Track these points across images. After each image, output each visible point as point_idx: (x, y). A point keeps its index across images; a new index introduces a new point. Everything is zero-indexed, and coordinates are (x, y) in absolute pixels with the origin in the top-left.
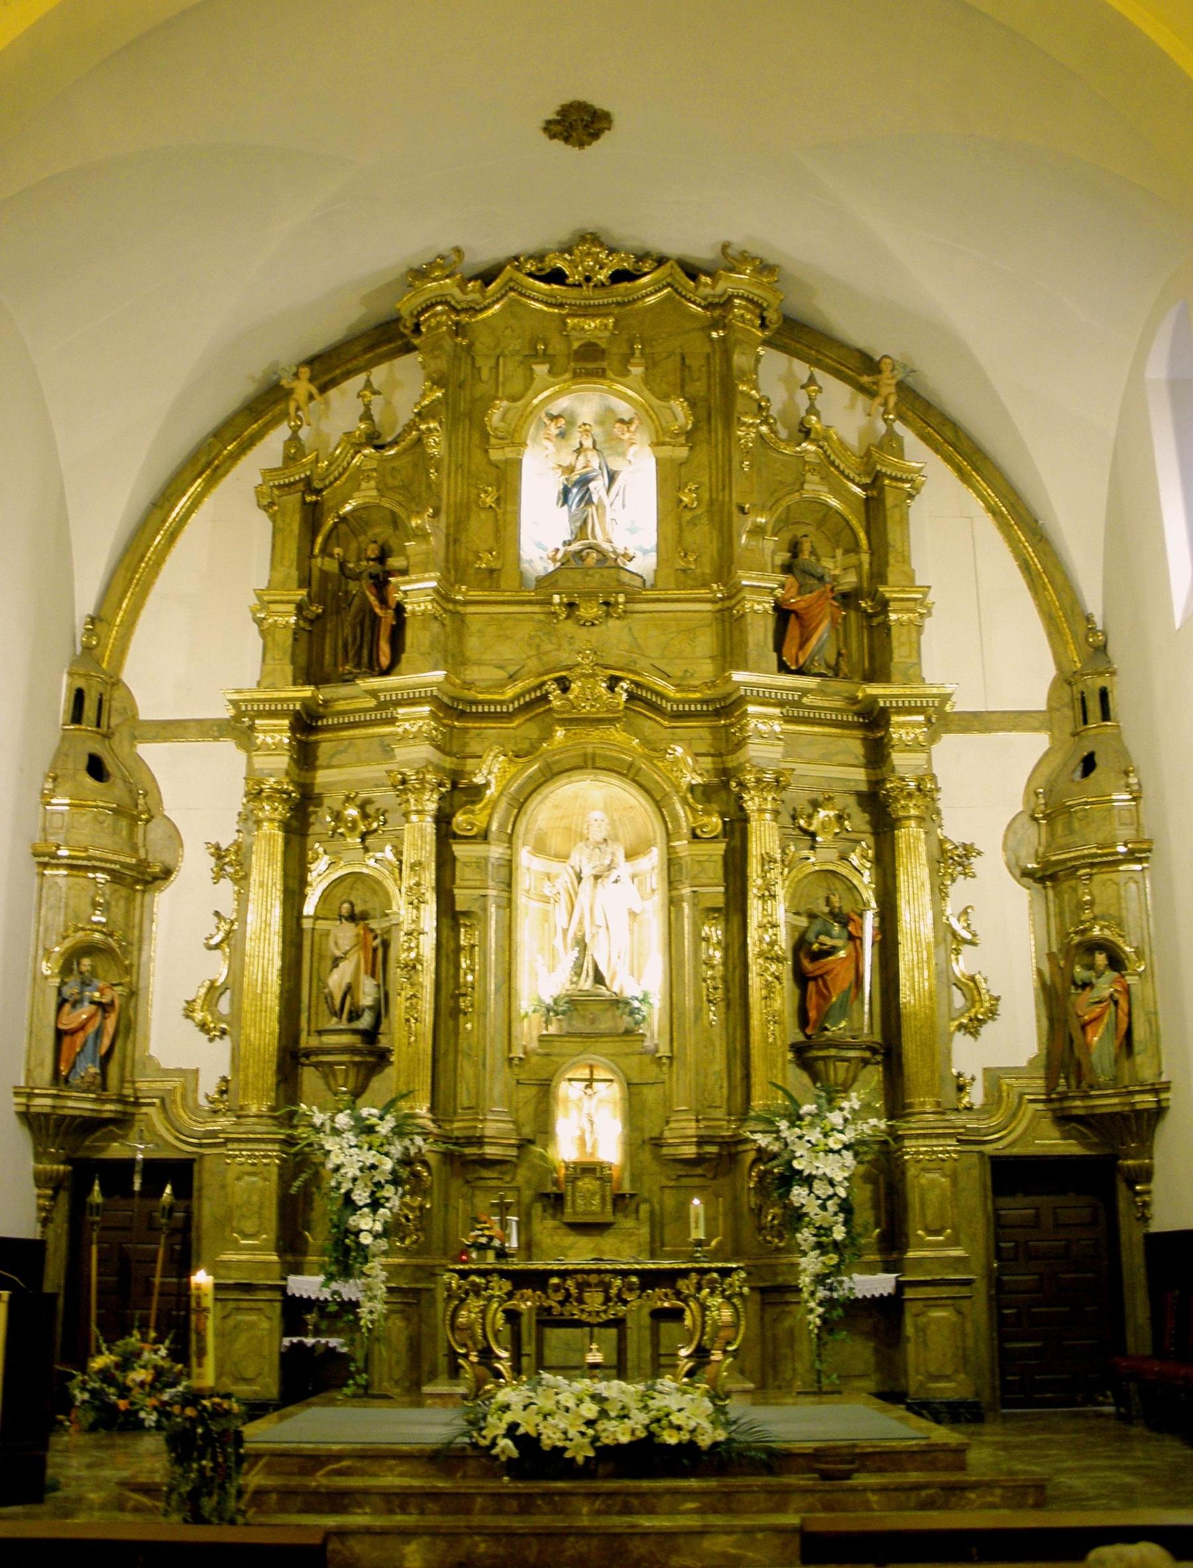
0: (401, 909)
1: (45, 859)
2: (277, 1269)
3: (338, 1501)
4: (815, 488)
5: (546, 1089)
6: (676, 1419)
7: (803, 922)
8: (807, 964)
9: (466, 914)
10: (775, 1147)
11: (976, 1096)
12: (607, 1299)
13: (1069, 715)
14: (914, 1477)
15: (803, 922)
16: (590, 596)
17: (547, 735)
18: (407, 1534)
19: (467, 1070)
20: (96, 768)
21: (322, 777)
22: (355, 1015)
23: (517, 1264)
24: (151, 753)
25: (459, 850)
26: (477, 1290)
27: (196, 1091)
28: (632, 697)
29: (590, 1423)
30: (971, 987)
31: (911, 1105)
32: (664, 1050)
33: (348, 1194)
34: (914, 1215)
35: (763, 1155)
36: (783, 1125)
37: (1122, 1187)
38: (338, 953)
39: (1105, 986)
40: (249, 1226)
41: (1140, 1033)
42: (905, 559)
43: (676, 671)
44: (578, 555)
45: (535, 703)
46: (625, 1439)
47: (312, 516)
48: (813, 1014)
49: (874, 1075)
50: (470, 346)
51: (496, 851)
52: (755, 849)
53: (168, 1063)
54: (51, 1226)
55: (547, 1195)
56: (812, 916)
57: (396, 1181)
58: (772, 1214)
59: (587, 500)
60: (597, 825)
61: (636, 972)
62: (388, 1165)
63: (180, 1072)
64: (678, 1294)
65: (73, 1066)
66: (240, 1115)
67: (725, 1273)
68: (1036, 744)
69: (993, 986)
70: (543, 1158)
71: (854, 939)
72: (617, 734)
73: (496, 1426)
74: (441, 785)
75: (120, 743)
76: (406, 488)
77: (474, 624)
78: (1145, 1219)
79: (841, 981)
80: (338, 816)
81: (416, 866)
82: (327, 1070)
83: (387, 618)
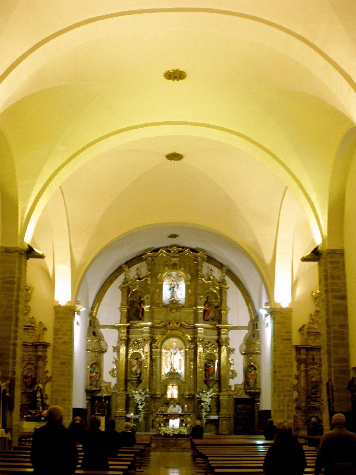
1: (87, 350)
6: (183, 431)
7: (206, 361)
9: (154, 360)
10: (200, 397)
11: (233, 389)
13: (251, 328)
16: (174, 309)
19: (154, 384)
20: (94, 334)
21: (131, 336)
22: (137, 374)
23: (164, 414)
24: (102, 330)
25: (153, 350)
26: (159, 416)
28: (180, 326)
29: (173, 432)
30: (233, 371)
31: (222, 390)
32: (184, 381)
35: (198, 398)
38: (134, 365)
39: (253, 373)
40: (121, 407)
41: (258, 380)
42: (226, 302)
43: (187, 321)
44: (172, 301)
46: (176, 434)
47: (129, 291)
48: (207, 376)
49: (217, 385)
51: (159, 350)
52: (199, 351)
54: (88, 407)
55: (166, 403)
56: (208, 360)
57: (144, 401)
58: (199, 406)
59: (173, 291)
61: (180, 369)
62: (144, 399)
63: (108, 383)
64: (183, 417)
67: (189, 415)
68: (246, 331)
69: (237, 371)
70: (165, 397)
71: (214, 364)
73: (162, 432)
74: (150, 340)
75: (97, 328)
78: (258, 408)
79: (211, 371)
81: (147, 353)
82: (132, 383)
83: (141, 310)
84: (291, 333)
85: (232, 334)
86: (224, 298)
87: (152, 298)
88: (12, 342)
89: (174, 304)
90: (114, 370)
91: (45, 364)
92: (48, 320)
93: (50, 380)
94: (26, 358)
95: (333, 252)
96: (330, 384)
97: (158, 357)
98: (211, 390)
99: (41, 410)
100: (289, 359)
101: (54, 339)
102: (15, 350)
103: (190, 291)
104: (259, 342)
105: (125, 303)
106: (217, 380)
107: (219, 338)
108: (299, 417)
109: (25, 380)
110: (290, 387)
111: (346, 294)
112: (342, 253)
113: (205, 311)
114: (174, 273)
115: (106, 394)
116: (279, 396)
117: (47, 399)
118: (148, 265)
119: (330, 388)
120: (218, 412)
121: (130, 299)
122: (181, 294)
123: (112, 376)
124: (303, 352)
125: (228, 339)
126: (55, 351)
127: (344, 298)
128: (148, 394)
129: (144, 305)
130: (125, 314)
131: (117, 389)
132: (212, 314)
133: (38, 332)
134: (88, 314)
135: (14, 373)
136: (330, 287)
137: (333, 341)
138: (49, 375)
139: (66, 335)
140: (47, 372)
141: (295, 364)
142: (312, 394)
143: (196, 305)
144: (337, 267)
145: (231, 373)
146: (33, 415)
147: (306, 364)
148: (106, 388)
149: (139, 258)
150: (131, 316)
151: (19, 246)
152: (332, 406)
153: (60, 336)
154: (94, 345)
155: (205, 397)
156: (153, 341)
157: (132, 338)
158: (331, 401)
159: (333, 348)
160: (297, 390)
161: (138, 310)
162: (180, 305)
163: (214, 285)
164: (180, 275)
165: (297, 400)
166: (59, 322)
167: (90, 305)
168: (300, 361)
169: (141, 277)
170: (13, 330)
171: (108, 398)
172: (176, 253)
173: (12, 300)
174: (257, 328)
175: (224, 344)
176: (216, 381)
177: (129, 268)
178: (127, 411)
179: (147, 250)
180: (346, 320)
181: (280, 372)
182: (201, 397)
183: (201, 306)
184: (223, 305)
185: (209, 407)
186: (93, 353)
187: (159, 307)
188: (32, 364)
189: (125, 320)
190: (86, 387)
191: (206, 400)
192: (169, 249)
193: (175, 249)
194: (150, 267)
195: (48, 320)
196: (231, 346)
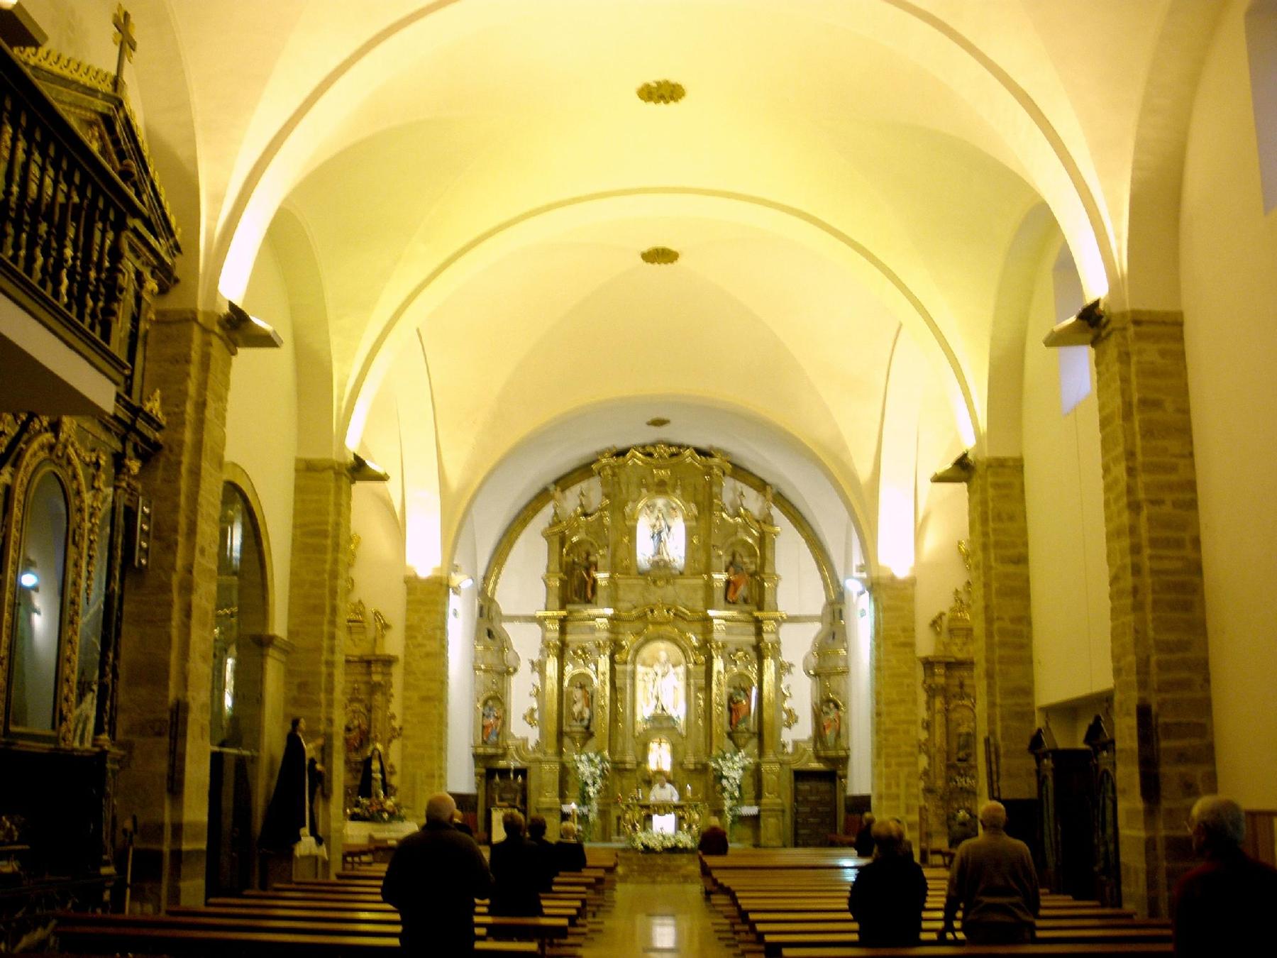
0: (596, 682)
1: (476, 668)
5: (645, 747)
7: (732, 690)
8: (732, 705)
9: (621, 688)
10: (717, 767)
13: (829, 619)
15: (732, 690)
16: (661, 578)
17: (646, 627)
24: (507, 627)
30: (790, 713)
32: (684, 733)
35: (715, 770)
36: (720, 760)
39: (832, 715)
41: (843, 730)
42: (773, 564)
43: (690, 604)
44: (657, 562)
45: (642, 617)
49: (755, 741)
51: (629, 667)
53: (518, 735)
56: (735, 688)
57: (600, 776)
59: (660, 540)
60: (663, 656)
66: (545, 753)
68: (817, 626)
71: (748, 697)
72: (668, 628)
75: (496, 623)
78: (844, 790)
80: (575, 653)
81: (604, 674)
82: (573, 740)
83: (590, 582)
85: (787, 632)
86: (768, 554)
88: (323, 658)
89: (661, 570)
91: (389, 701)
92: (393, 608)
96: (992, 741)
97: (628, 681)
100: (908, 686)
101: (407, 646)
102: (330, 675)
110: (913, 746)
111: (1027, 552)
113: (728, 582)
114: (660, 502)
116: (888, 765)
117: (392, 773)
119: (992, 749)
120: (758, 797)
121: (565, 559)
122: (676, 550)
126: (408, 671)
127: (1022, 560)
129: (596, 570)
132: (743, 590)
135: (330, 721)
136: (992, 538)
139: (432, 638)
140: (393, 717)
141: (922, 697)
142: (959, 760)
145: (785, 716)
147: (945, 697)
149: (584, 470)
151: (334, 457)
152: (995, 787)
153: (420, 639)
154: (491, 659)
156: (616, 647)
159: (997, 667)
160: (927, 753)
163: (746, 527)
165: (926, 773)
167: (481, 572)
168: (932, 692)
169: (589, 511)
171: (522, 772)
177: (563, 491)
178: (563, 797)
179: (602, 453)
180: (1027, 606)
183: (720, 572)
184: (767, 570)
188: (360, 701)
190: (475, 747)
195: (393, 608)
196: (786, 657)
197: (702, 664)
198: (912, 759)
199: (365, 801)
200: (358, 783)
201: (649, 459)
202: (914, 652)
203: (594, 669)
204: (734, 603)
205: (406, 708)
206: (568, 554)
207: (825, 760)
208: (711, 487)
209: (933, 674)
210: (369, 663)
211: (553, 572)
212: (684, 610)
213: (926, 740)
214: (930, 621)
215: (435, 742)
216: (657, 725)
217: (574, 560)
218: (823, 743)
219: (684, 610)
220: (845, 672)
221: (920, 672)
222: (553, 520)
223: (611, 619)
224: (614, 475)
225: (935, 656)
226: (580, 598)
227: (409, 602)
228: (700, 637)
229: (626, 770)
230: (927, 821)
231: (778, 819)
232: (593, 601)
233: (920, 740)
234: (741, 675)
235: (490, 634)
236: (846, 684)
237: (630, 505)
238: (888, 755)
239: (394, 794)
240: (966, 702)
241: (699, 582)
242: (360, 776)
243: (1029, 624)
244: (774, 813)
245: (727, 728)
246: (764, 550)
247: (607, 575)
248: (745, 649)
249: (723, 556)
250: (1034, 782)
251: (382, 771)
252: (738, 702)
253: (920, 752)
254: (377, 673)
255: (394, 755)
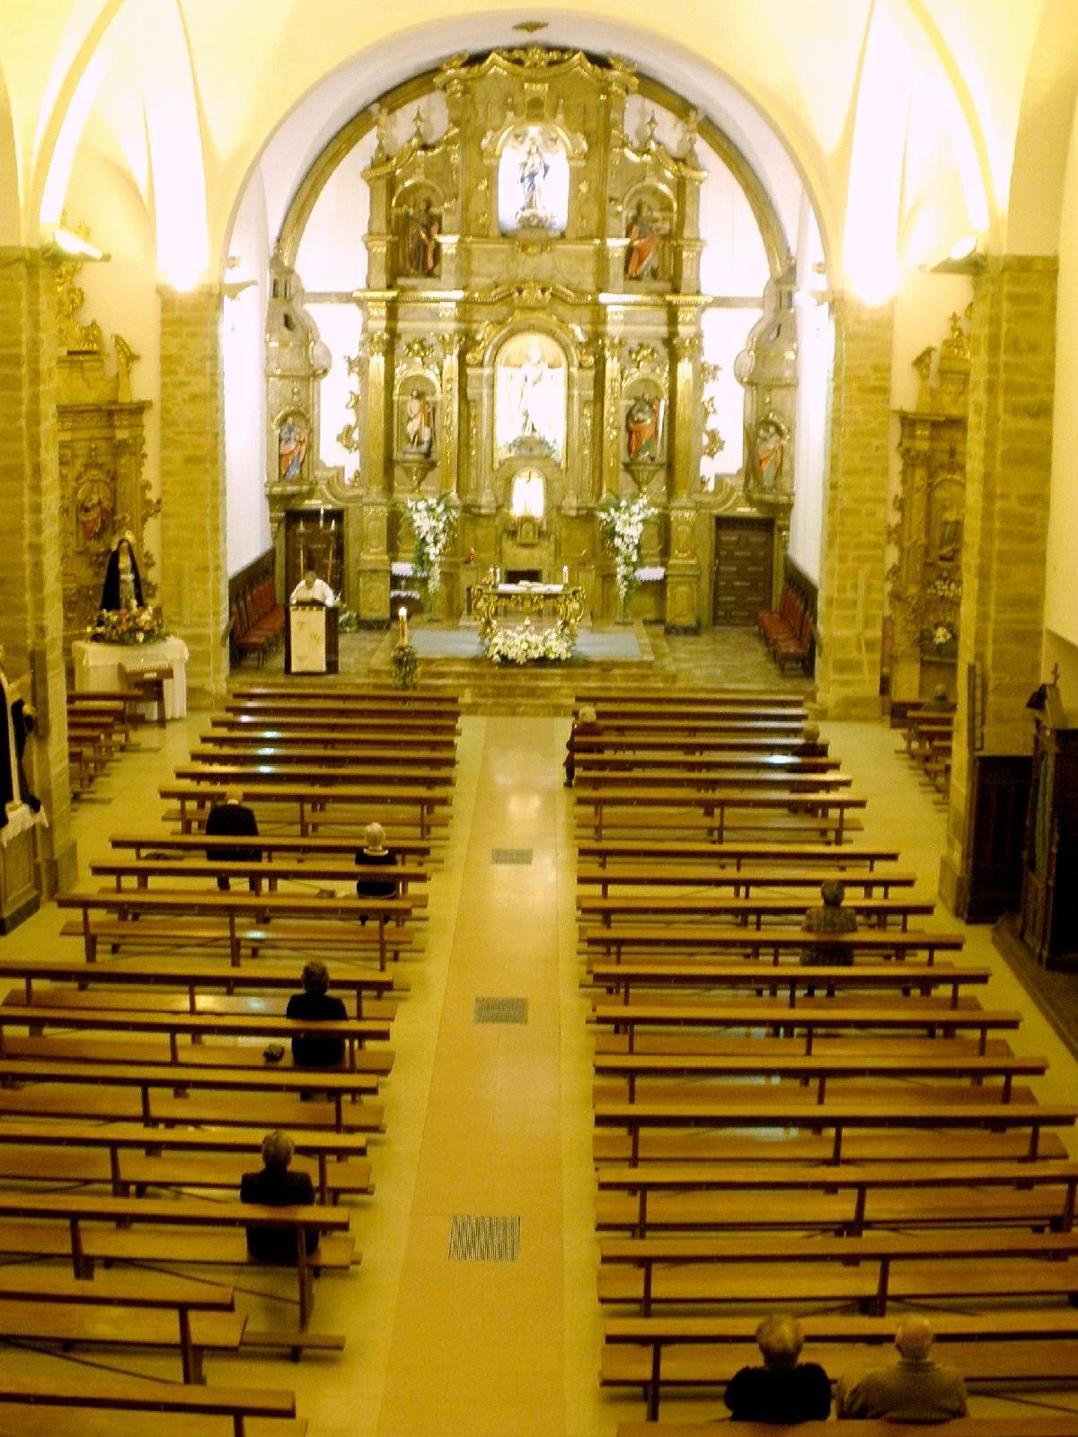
1: (268, 375)
2: (388, 563)
3: (441, 675)
4: (651, 180)
5: (509, 482)
8: (632, 425)
9: (474, 401)
12: (532, 604)
14: (634, 671)
16: (533, 243)
17: (511, 314)
18: (465, 686)
24: (310, 308)
27: (343, 477)
28: (553, 295)
30: (713, 436)
33: (424, 539)
34: (673, 545)
36: (612, 511)
37: (776, 530)
39: (771, 444)
40: (375, 543)
41: (786, 467)
43: (575, 281)
47: (392, 184)
48: (634, 448)
49: (661, 475)
50: (472, 100)
51: (487, 371)
52: (608, 375)
53: (330, 464)
54: (277, 541)
56: (637, 399)
59: (532, 187)
60: (535, 357)
62: (441, 525)
63: (335, 468)
65: (288, 470)
69: (722, 436)
70: (508, 514)
71: (655, 412)
72: (541, 315)
73: (493, 651)
76: (440, 174)
77: (476, 254)
81: (449, 381)
82: (408, 471)
84: (889, 369)
85: (712, 322)
86: (688, 209)
87: (465, 209)
88: (26, 541)
89: (533, 234)
90: (349, 430)
91: (140, 465)
92: (143, 333)
93: (157, 511)
94: (81, 449)
95: (1022, 266)
96: (978, 670)
97: (485, 391)
98: (644, 501)
99: (135, 609)
100: (877, 448)
101: (164, 386)
102: (37, 565)
103: (584, 187)
104: (796, 353)
105: (381, 225)
106: (664, 459)
107: (673, 334)
108: (900, 623)
109: (83, 517)
110: (879, 534)
111: (1052, 401)
112: (1049, 269)
113: (630, 251)
114: (534, 130)
115: (330, 502)
116: (843, 559)
117: (149, 565)
118: (452, 104)
119: (978, 681)
120: (665, 553)
121: (395, 211)
122: (555, 206)
123: (346, 446)
124: (921, 432)
125: (699, 335)
126: (166, 423)
127: (1043, 411)
128: (455, 508)
129: (440, 232)
130: (381, 261)
131: (361, 485)
132: (651, 260)
133: (112, 365)
134: (267, 262)
135: (41, 630)
136: (1003, 376)
137: (997, 545)
138: (152, 495)
139: (199, 372)
140: (147, 486)
141: (896, 464)
142: (942, 558)
143: (602, 235)
144: (1030, 315)
145: (705, 440)
146: (114, 627)
147: (929, 468)
148: (329, 485)
149: (424, 80)
150: (401, 262)
151: (24, 242)
152: (978, 734)
153: (181, 376)
154: (291, 361)
155: (625, 522)
156: (468, 341)
157: (405, 331)
158: (978, 721)
159: (995, 566)
160: (899, 543)
161: (422, 247)
162: (552, 234)
163: (658, 167)
164: (554, 136)
165: (895, 571)
166: (175, 335)
167: (274, 232)
168: (911, 459)
169: (430, 141)
170: (27, 506)
171: (337, 515)
172: (542, 68)
173: (18, 416)
174: (790, 306)
175: (687, 354)
176: (661, 465)
177: (392, 111)
178: (393, 550)
179: (448, 60)
180: (1046, 480)
181: (849, 488)
182: (613, 520)
183: (618, 237)
184: (687, 233)
185: (635, 551)
186: (287, 382)
187: (487, 236)
188: (100, 466)
189: (382, 280)
190: (270, 484)
191: (628, 531)
192: (516, 54)
193: (536, 55)
194: (457, 114)
195: (143, 333)
196: (709, 357)
197: (590, 368)
198: (877, 552)
199: (113, 617)
200: (102, 581)
201: (518, 69)
202: (888, 401)
203: (437, 371)
204: (638, 278)
205: (166, 474)
206: (399, 205)
207: (760, 504)
208: (608, 113)
209: (913, 436)
210: (110, 414)
211: (379, 234)
212: (565, 290)
213: (898, 526)
214: (914, 358)
215: (208, 522)
216: (524, 451)
217: (407, 213)
218: (759, 482)
219: (565, 290)
220: (792, 385)
221: (895, 430)
222: (376, 154)
223: (460, 303)
224: (465, 92)
225: (915, 414)
226: (417, 268)
227: (164, 323)
228: (588, 328)
229: (480, 515)
230: (893, 639)
231: (691, 588)
232: (436, 271)
233: (889, 526)
234: (645, 381)
235: (288, 322)
236: (794, 403)
237: (489, 134)
238: (843, 546)
239: (152, 596)
240: (957, 477)
241: (589, 248)
242: (104, 572)
243: (1046, 505)
244: (685, 579)
245: (624, 457)
246: (684, 204)
247: (454, 239)
248: (652, 345)
249: (625, 211)
250: (1032, 743)
251: (134, 569)
252: (638, 422)
253: (889, 542)
254: (120, 427)
255: (151, 538)
